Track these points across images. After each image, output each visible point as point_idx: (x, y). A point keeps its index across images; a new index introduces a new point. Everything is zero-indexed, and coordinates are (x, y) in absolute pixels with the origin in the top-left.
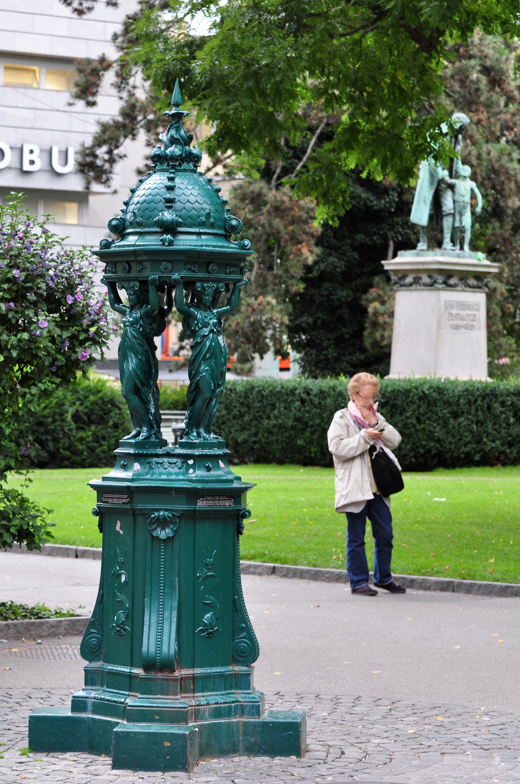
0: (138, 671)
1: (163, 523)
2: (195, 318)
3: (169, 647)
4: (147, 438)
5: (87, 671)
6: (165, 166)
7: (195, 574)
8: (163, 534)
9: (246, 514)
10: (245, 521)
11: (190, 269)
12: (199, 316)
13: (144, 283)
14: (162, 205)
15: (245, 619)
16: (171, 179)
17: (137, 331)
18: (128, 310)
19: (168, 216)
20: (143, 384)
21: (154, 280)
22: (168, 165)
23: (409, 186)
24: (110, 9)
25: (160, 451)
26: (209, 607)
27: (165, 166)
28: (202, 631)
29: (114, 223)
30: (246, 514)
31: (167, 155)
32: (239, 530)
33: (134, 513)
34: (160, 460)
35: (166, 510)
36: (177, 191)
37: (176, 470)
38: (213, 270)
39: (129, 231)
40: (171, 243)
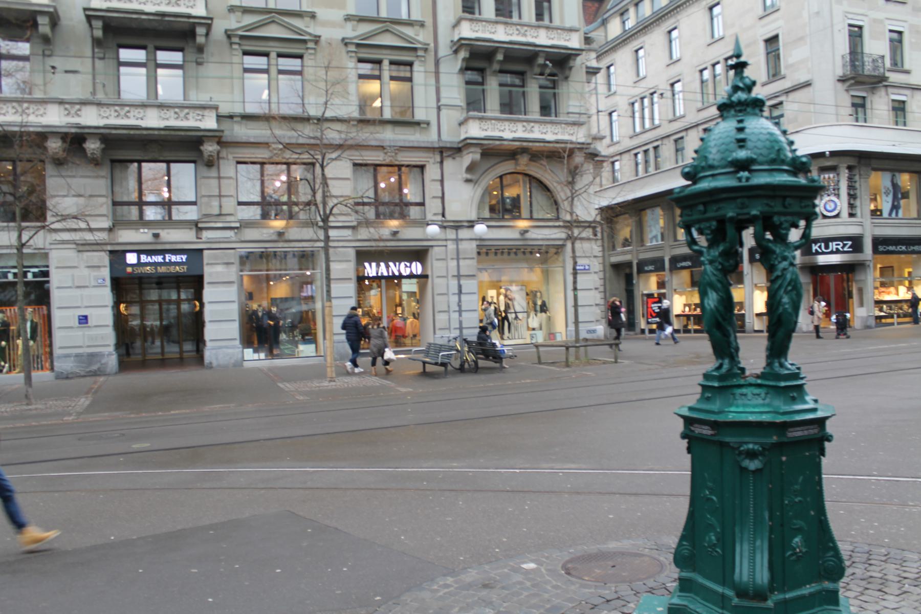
0: (730, 593)
1: (752, 455)
2: (774, 252)
3: (763, 576)
4: (729, 370)
5: (681, 580)
6: (733, 112)
7: (783, 501)
8: (753, 465)
9: (829, 438)
10: (827, 444)
11: (767, 205)
12: (778, 251)
13: (722, 221)
14: (734, 146)
15: (831, 539)
16: (740, 121)
17: (717, 269)
18: (705, 250)
19: (742, 154)
20: (724, 319)
21: (731, 219)
22: (736, 111)
23: (703, 295)
24: (658, 347)
25: (742, 382)
26: (799, 530)
27: (733, 112)
28: (792, 555)
29: (687, 170)
30: (829, 438)
31: (732, 102)
32: (822, 452)
33: (723, 445)
34: (744, 390)
35: (755, 443)
36: (747, 131)
37: (760, 401)
38: (790, 205)
39: (702, 175)
40: (748, 179)
